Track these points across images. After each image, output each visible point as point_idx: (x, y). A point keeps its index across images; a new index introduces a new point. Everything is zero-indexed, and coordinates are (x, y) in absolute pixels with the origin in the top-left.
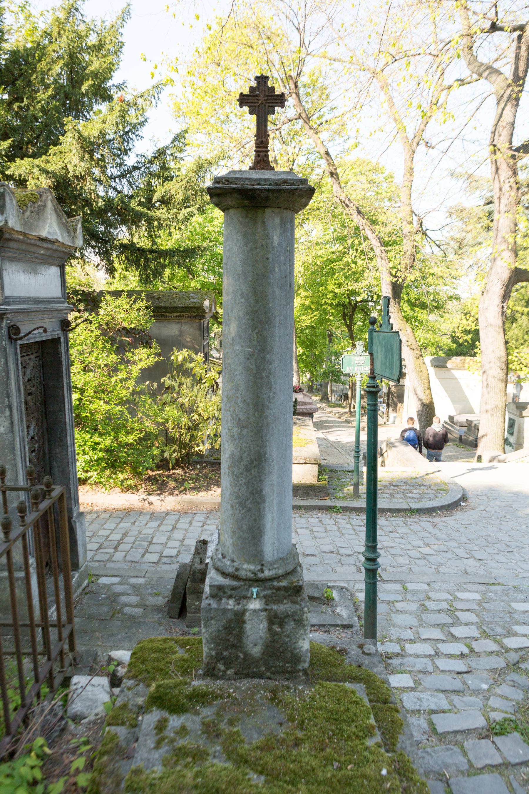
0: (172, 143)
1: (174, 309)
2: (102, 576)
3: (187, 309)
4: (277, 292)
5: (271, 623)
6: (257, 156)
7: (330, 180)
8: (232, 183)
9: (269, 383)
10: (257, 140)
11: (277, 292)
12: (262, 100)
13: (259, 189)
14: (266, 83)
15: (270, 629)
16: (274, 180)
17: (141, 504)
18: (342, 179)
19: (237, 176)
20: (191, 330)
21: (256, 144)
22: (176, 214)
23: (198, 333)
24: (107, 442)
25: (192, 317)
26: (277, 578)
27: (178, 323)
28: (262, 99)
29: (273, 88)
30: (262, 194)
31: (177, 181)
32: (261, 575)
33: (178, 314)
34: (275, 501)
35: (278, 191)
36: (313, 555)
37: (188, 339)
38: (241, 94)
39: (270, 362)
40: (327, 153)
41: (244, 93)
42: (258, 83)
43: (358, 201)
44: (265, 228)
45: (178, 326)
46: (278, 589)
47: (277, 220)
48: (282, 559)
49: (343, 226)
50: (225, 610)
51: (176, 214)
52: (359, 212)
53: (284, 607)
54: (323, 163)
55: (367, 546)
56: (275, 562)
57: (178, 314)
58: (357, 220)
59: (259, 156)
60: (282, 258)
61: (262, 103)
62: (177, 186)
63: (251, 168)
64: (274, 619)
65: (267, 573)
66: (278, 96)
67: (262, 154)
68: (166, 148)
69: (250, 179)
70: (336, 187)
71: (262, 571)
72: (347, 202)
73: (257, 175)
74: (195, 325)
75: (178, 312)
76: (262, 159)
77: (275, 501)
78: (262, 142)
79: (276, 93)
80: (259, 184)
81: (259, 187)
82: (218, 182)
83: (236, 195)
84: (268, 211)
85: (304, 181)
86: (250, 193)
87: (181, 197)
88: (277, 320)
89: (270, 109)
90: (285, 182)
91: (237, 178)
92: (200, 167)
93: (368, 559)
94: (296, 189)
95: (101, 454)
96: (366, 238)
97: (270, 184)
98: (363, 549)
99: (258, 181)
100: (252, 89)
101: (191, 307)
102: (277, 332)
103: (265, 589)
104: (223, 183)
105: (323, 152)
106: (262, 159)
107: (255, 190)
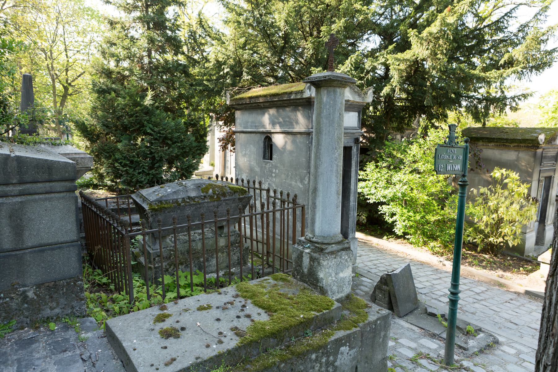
1: (513, 141)
2: (512, 355)
3: (524, 141)
4: (325, 121)
5: (310, 260)
9: (320, 158)
11: (325, 121)
15: (310, 263)
17: (437, 263)
20: (527, 157)
23: (532, 159)
24: (418, 217)
25: (528, 147)
26: (318, 243)
27: (516, 151)
32: (312, 239)
33: (516, 144)
34: (321, 209)
36: (516, 324)
37: (523, 164)
39: (320, 150)
44: (321, 95)
45: (516, 153)
46: (316, 247)
47: (326, 92)
48: (324, 237)
50: (298, 249)
53: (315, 255)
55: (452, 284)
56: (320, 236)
57: (516, 144)
60: (328, 107)
64: (312, 259)
65: (314, 239)
71: (313, 238)
74: (530, 153)
75: (516, 142)
77: (321, 209)
84: (322, 89)
88: (324, 132)
93: (452, 293)
95: (411, 223)
98: (449, 285)
101: (527, 140)
102: (324, 137)
103: (312, 246)
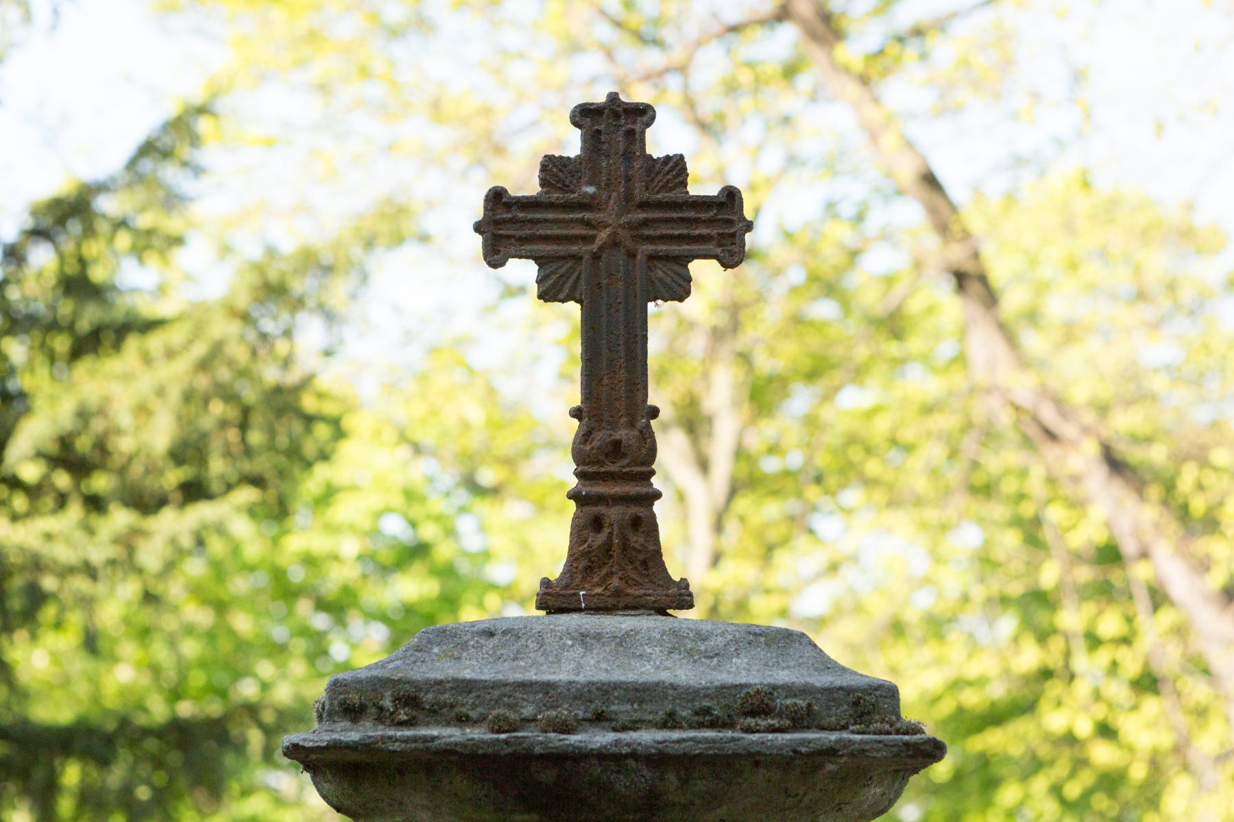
0: (132, 164)
6: (588, 524)
7: (951, 307)
8: (436, 713)
10: (584, 437)
12: (612, 224)
13: (603, 756)
14: (635, 139)
16: (691, 694)
18: (1013, 301)
19: (471, 669)
21: (580, 456)
22: (128, 541)
28: (612, 220)
29: (676, 167)
30: (621, 784)
31: (147, 359)
35: (722, 764)
38: (496, 198)
40: (930, 181)
41: (514, 192)
42: (593, 141)
43: (1103, 410)
49: (1032, 532)
51: (128, 541)
52: (1114, 463)
54: (910, 213)
58: (1107, 511)
59: (597, 523)
61: (614, 243)
62: (145, 383)
63: (554, 599)
66: (703, 203)
67: (613, 514)
68: (101, 188)
69: (547, 687)
70: (984, 345)
72: (1048, 414)
73: (586, 655)
76: (616, 555)
78: (616, 449)
79: (695, 189)
80: (599, 719)
81: (601, 738)
82: (353, 712)
83: (460, 783)
85: (873, 702)
86: (548, 776)
87: (160, 435)
89: (661, 272)
90: (758, 705)
91: (466, 686)
92: (273, 291)
94: (830, 752)
96: (1158, 598)
97: (671, 722)
99: (599, 704)
100: (553, 169)
104: (382, 716)
105: (907, 173)
106: (616, 555)
107: (579, 757)
